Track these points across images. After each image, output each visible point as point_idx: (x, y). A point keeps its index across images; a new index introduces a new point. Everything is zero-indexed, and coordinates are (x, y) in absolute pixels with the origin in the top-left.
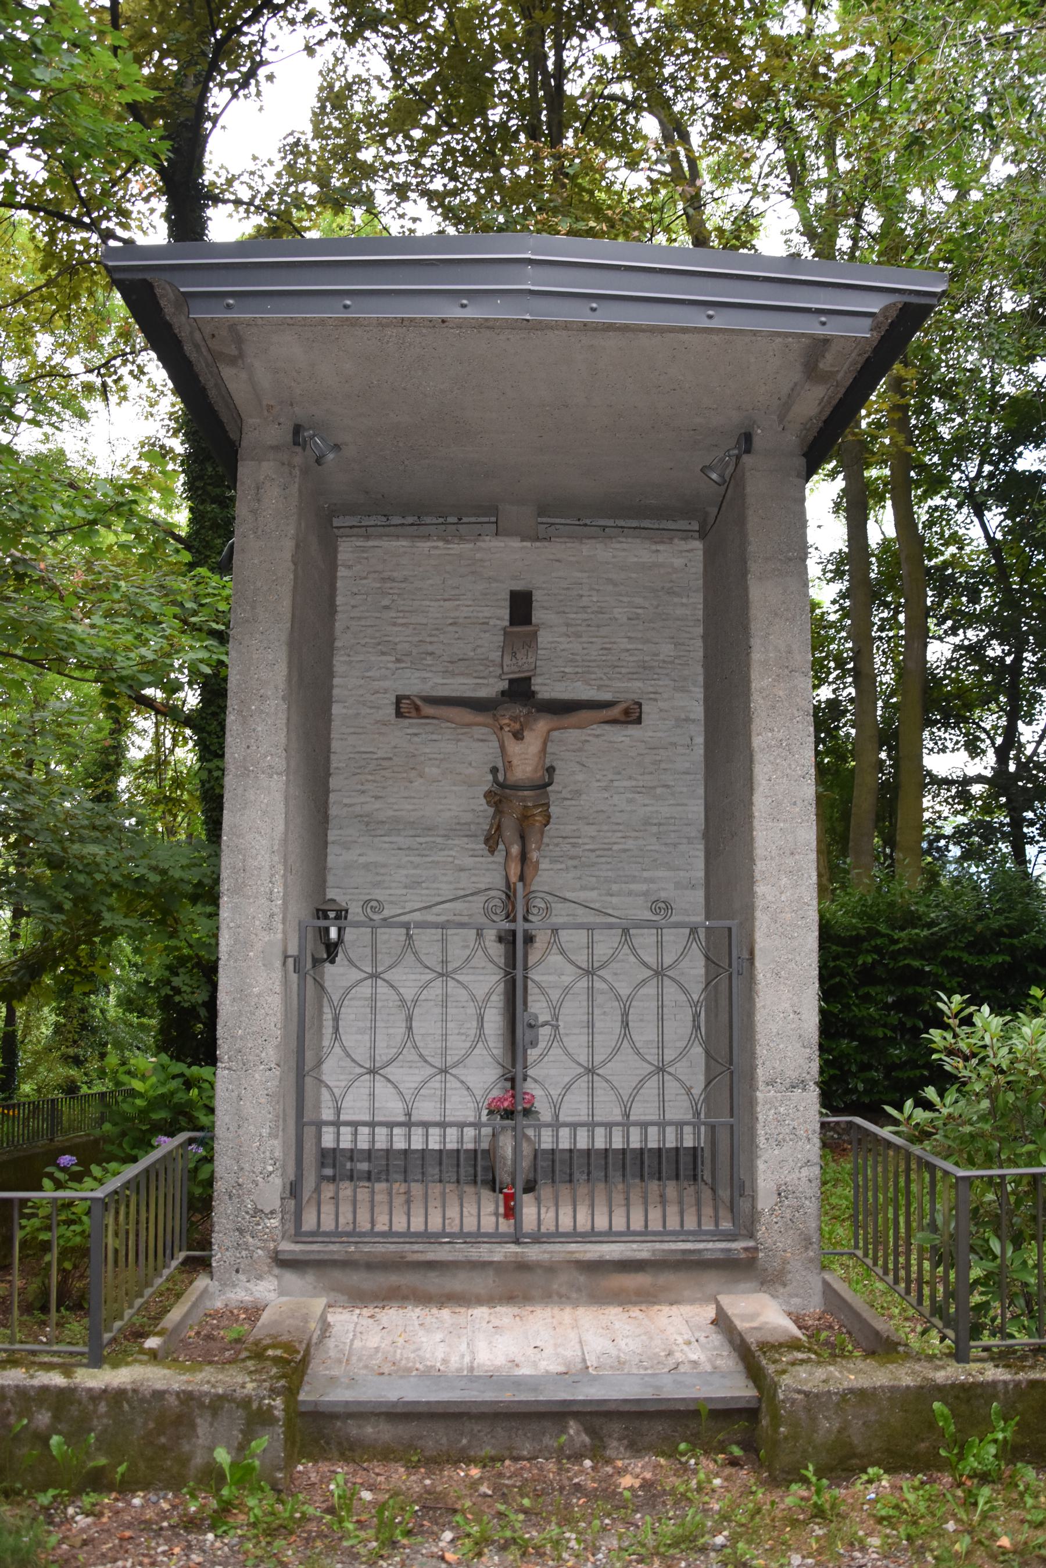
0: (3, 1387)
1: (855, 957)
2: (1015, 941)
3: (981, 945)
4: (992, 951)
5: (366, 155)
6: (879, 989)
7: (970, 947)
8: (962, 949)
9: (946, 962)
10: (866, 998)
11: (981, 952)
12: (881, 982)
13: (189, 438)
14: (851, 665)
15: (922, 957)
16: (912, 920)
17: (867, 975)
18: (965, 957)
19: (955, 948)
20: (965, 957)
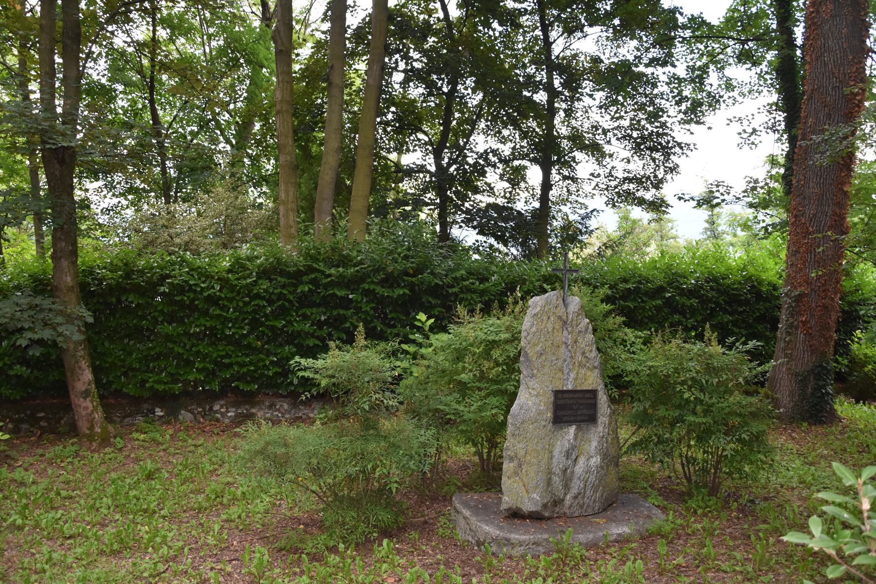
0: (874, 401)
1: (296, 286)
2: (413, 279)
3: (390, 281)
4: (399, 286)
5: (140, 106)
6: (314, 310)
7: (383, 283)
8: (377, 284)
9: (367, 293)
10: (305, 317)
11: (391, 286)
12: (314, 305)
13: (63, 58)
14: (569, 10)
15: (348, 287)
16: (345, 261)
17: (304, 301)
18: (379, 290)
19: (372, 282)
20: (379, 290)
